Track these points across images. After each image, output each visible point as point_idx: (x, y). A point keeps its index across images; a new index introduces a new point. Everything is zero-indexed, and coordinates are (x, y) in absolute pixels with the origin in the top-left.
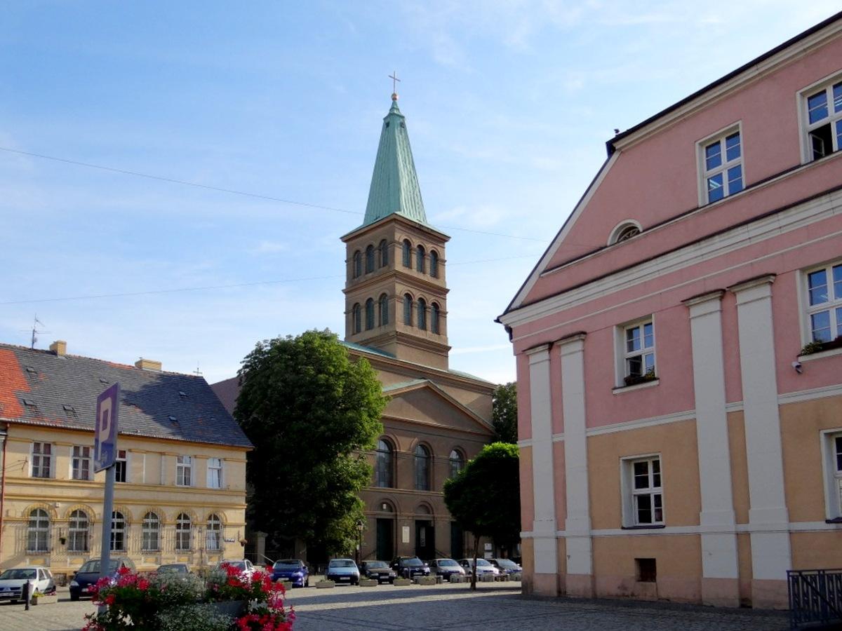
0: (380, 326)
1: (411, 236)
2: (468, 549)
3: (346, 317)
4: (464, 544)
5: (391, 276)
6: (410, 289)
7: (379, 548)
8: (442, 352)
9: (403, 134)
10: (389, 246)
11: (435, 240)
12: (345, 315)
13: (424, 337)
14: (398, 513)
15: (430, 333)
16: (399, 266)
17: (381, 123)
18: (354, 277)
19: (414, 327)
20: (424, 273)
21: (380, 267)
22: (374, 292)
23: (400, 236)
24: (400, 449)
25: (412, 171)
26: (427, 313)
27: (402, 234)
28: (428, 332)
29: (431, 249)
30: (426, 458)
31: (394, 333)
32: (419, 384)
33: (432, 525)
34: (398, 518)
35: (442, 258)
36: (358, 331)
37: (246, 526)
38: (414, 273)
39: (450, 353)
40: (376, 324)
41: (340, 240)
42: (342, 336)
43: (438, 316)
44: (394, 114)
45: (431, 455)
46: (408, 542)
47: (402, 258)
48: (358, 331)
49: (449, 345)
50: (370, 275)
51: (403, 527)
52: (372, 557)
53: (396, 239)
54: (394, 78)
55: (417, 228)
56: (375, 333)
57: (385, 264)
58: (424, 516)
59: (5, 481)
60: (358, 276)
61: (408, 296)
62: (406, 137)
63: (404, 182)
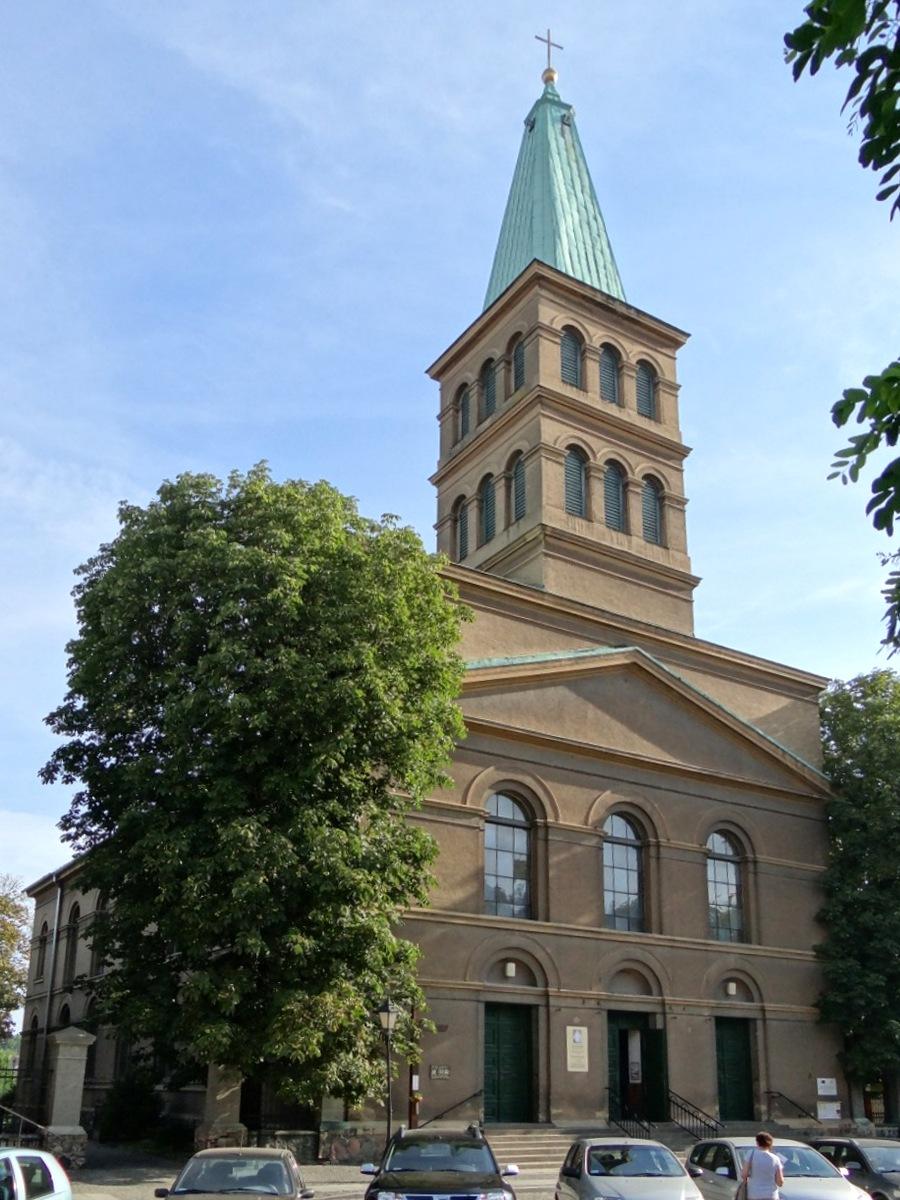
0: (507, 528)
1: (580, 319)
2: (769, 1092)
4: (757, 1079)
5: (530, 405)
7: (492, 1086)
11: (650, 339)
14: (552, 990)
19: (596, 525)
20: (621, 405)
21: (507, 396)
24: (557, 817)
25: (590, 206)
28: (634, 539)
30: (639, 849)
31: (538, 531)
34: (552, 1001)
35: (668, 377)
38: (593, 398)
39: (696, 592)
43: (662, 507)
44: (549, 101)
45: (652, 840)
46: (586, 1069)
49: (694, 572)
50: (487, 424)
51: (570, 1029)
52: (470, 1113)
54: (548, 42)
58: (632, 999)
59: (768, 1015)
62: (576, 143)
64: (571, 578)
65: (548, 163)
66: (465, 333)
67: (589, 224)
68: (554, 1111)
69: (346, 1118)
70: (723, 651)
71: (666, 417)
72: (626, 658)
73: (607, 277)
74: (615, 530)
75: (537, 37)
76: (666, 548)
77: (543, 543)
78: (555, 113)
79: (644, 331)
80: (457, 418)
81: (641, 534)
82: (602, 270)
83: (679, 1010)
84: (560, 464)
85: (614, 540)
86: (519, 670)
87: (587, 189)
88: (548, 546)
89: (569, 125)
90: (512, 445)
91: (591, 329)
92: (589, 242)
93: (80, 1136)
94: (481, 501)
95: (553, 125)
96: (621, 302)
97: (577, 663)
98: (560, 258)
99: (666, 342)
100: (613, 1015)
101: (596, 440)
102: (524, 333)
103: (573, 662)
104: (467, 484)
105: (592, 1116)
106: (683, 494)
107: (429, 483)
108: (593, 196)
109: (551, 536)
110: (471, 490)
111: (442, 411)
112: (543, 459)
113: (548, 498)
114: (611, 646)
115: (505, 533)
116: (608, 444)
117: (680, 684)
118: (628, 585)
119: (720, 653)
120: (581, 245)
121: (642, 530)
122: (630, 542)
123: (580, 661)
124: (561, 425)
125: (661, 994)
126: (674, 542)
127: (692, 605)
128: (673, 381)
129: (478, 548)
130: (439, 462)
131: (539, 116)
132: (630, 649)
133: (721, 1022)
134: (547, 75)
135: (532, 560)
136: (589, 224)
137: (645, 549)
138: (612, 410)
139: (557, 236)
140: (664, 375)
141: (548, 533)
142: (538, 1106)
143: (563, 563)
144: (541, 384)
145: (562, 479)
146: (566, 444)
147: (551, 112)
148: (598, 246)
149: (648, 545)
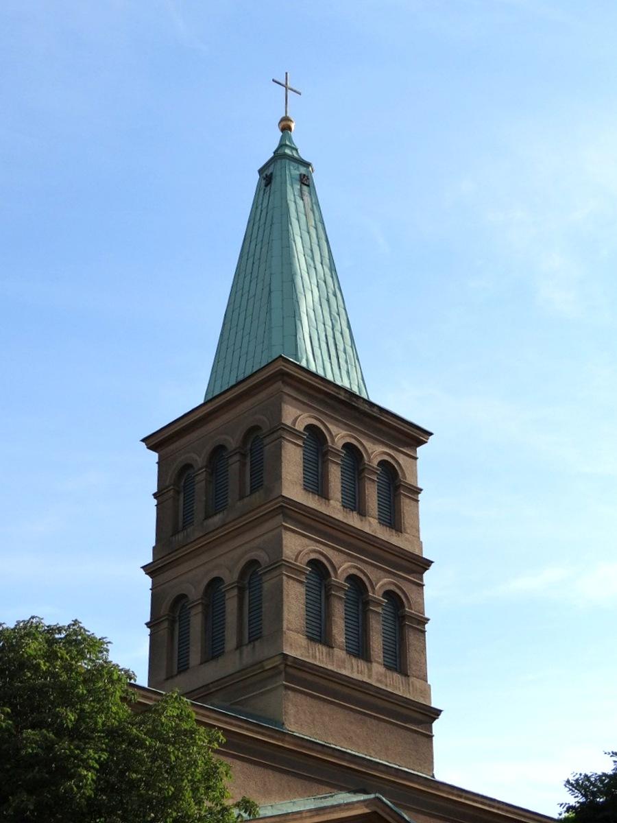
0: (239, 646)
3: (153, 637)
8: (410, 572)
9: (307, 198)
10: (267, 440)
12: (157, 465)
13: (366, 679)
15: (382, 669)
16: (293, 487)
17: (253, 180)
18: (176, 532)
20: (362, 513)
21: (242, 497)
23: (296, 416)
25: (329, 280)
26: (371, 616)
27: (304, 411)
28: (375, 665)
31: (277, 661)
32: (349, 805)
35: (409, 480)
36: (183, 668)
38: (334, 509)
40: (231, 642)
41: (146, 626)
42: (142, 680)
44: (285, 156)
47: (300, 470)
48: (183, 668)
49: (435, 704)
50: (217, 519)
53: (288, 421)
54: (286, 86)
55: (342, 402)
56: (228, 665)
57: (255, 636)
60: (184, 528)
61: (319, 569)
62: (316, 204)
63: (309, 301)
64: (311, 713)
65: (288, 230)
67: (328, 300)
70: (464, 794)
71: (407, 525)
72: (367, 807)
73: (347, 362)
74: (355, 656)
75: (273, 80)
76: (406, 675)
77: (283, 674)
78: (295, 171)
79: (384, 428)
80: (178, 500)
81: (381, 660)
82: (341, 354)
84: (301, 582)
85: (353, 669)
87: (327, 261)
88: (290, 678)
89: (308, 186)
90: (246, 553)
91: (334, 429)
92: (329, 323)
94: (206, 607)
95: (292, 186)
96: (364, 399)
97: (317, 815)
98: (301, 354)
99: (408, 440)
101: (336, 553)
103: (314, 813)
106: (423, 613)
108: (333, 269)
109: (291, 666)
112: (285, 578)
113: (288, 620)
114: (349, 791)
116: (349, 559)
118: (368, 719)
119: (460, 797)
120: (321, 327)
121: (381, 655)
122: (370, 670)
123: (321, 812)
124: (302, 538)
127: (432, 740)
128: (417, 552)
129: (201, 664)
131: (276, 169)
132: (372, 796)
134: (284, 123)
136: (328, 300)
138: (354, 520)
139: (297, 318)
140: (405, 478)
141: (289, 663)
143: (303, 696)
144: (283, 494)
145: (302, 599)
146: (306, 560)
147: (289, 169)
148: (338, 327)
149: (389, 673)
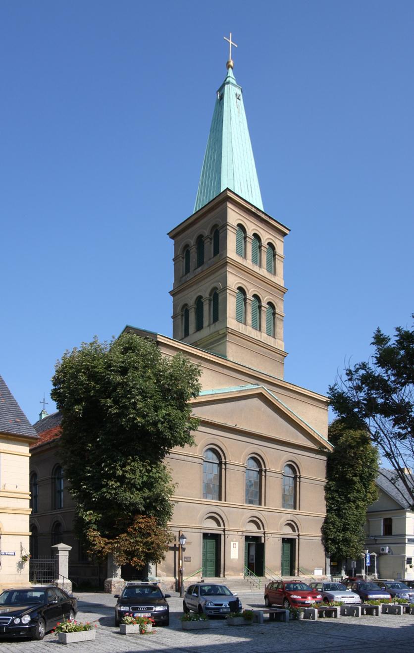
6: (243, 282)
16: (232, 323)
22: (204, 289)
28: (263, 333)
29: (267, 243)
33: (263, 541)
37: (31, 536)
38: (248, 263)
58: (252, 530)
66: (188, 219)
68: (226, 573)
69: (156, 576)
81: (265, 332)
83: (270, 535)
86: (218, 396)
93: (69, 583)
97: (240, 393)
100: (247, 538)
102: (220, 226)
104: (190, 298)
105: (239, 575)
107: (169, 294)
110: (191, 302)
111: (175, 257)
115: (209, 328)
117: (278, 402)
122: (261, 336)
125: (264, 529)
126: (278, 335)
129: (196, 332)
130: (174, 284)
133: (285, 541)
135: (222, 343)
137: (267, 338)
142: (220, 571)
